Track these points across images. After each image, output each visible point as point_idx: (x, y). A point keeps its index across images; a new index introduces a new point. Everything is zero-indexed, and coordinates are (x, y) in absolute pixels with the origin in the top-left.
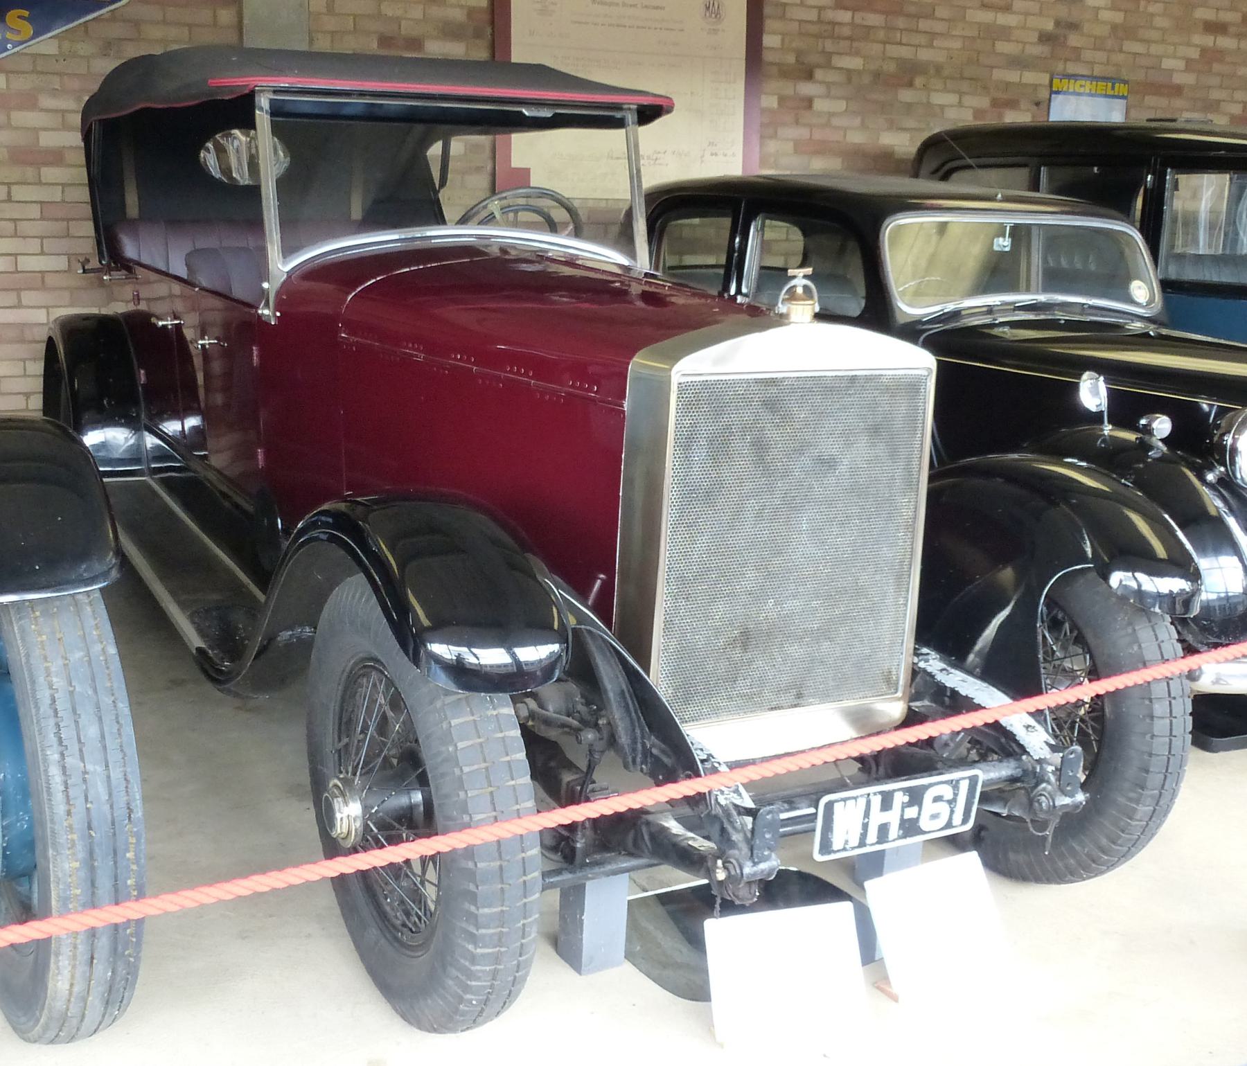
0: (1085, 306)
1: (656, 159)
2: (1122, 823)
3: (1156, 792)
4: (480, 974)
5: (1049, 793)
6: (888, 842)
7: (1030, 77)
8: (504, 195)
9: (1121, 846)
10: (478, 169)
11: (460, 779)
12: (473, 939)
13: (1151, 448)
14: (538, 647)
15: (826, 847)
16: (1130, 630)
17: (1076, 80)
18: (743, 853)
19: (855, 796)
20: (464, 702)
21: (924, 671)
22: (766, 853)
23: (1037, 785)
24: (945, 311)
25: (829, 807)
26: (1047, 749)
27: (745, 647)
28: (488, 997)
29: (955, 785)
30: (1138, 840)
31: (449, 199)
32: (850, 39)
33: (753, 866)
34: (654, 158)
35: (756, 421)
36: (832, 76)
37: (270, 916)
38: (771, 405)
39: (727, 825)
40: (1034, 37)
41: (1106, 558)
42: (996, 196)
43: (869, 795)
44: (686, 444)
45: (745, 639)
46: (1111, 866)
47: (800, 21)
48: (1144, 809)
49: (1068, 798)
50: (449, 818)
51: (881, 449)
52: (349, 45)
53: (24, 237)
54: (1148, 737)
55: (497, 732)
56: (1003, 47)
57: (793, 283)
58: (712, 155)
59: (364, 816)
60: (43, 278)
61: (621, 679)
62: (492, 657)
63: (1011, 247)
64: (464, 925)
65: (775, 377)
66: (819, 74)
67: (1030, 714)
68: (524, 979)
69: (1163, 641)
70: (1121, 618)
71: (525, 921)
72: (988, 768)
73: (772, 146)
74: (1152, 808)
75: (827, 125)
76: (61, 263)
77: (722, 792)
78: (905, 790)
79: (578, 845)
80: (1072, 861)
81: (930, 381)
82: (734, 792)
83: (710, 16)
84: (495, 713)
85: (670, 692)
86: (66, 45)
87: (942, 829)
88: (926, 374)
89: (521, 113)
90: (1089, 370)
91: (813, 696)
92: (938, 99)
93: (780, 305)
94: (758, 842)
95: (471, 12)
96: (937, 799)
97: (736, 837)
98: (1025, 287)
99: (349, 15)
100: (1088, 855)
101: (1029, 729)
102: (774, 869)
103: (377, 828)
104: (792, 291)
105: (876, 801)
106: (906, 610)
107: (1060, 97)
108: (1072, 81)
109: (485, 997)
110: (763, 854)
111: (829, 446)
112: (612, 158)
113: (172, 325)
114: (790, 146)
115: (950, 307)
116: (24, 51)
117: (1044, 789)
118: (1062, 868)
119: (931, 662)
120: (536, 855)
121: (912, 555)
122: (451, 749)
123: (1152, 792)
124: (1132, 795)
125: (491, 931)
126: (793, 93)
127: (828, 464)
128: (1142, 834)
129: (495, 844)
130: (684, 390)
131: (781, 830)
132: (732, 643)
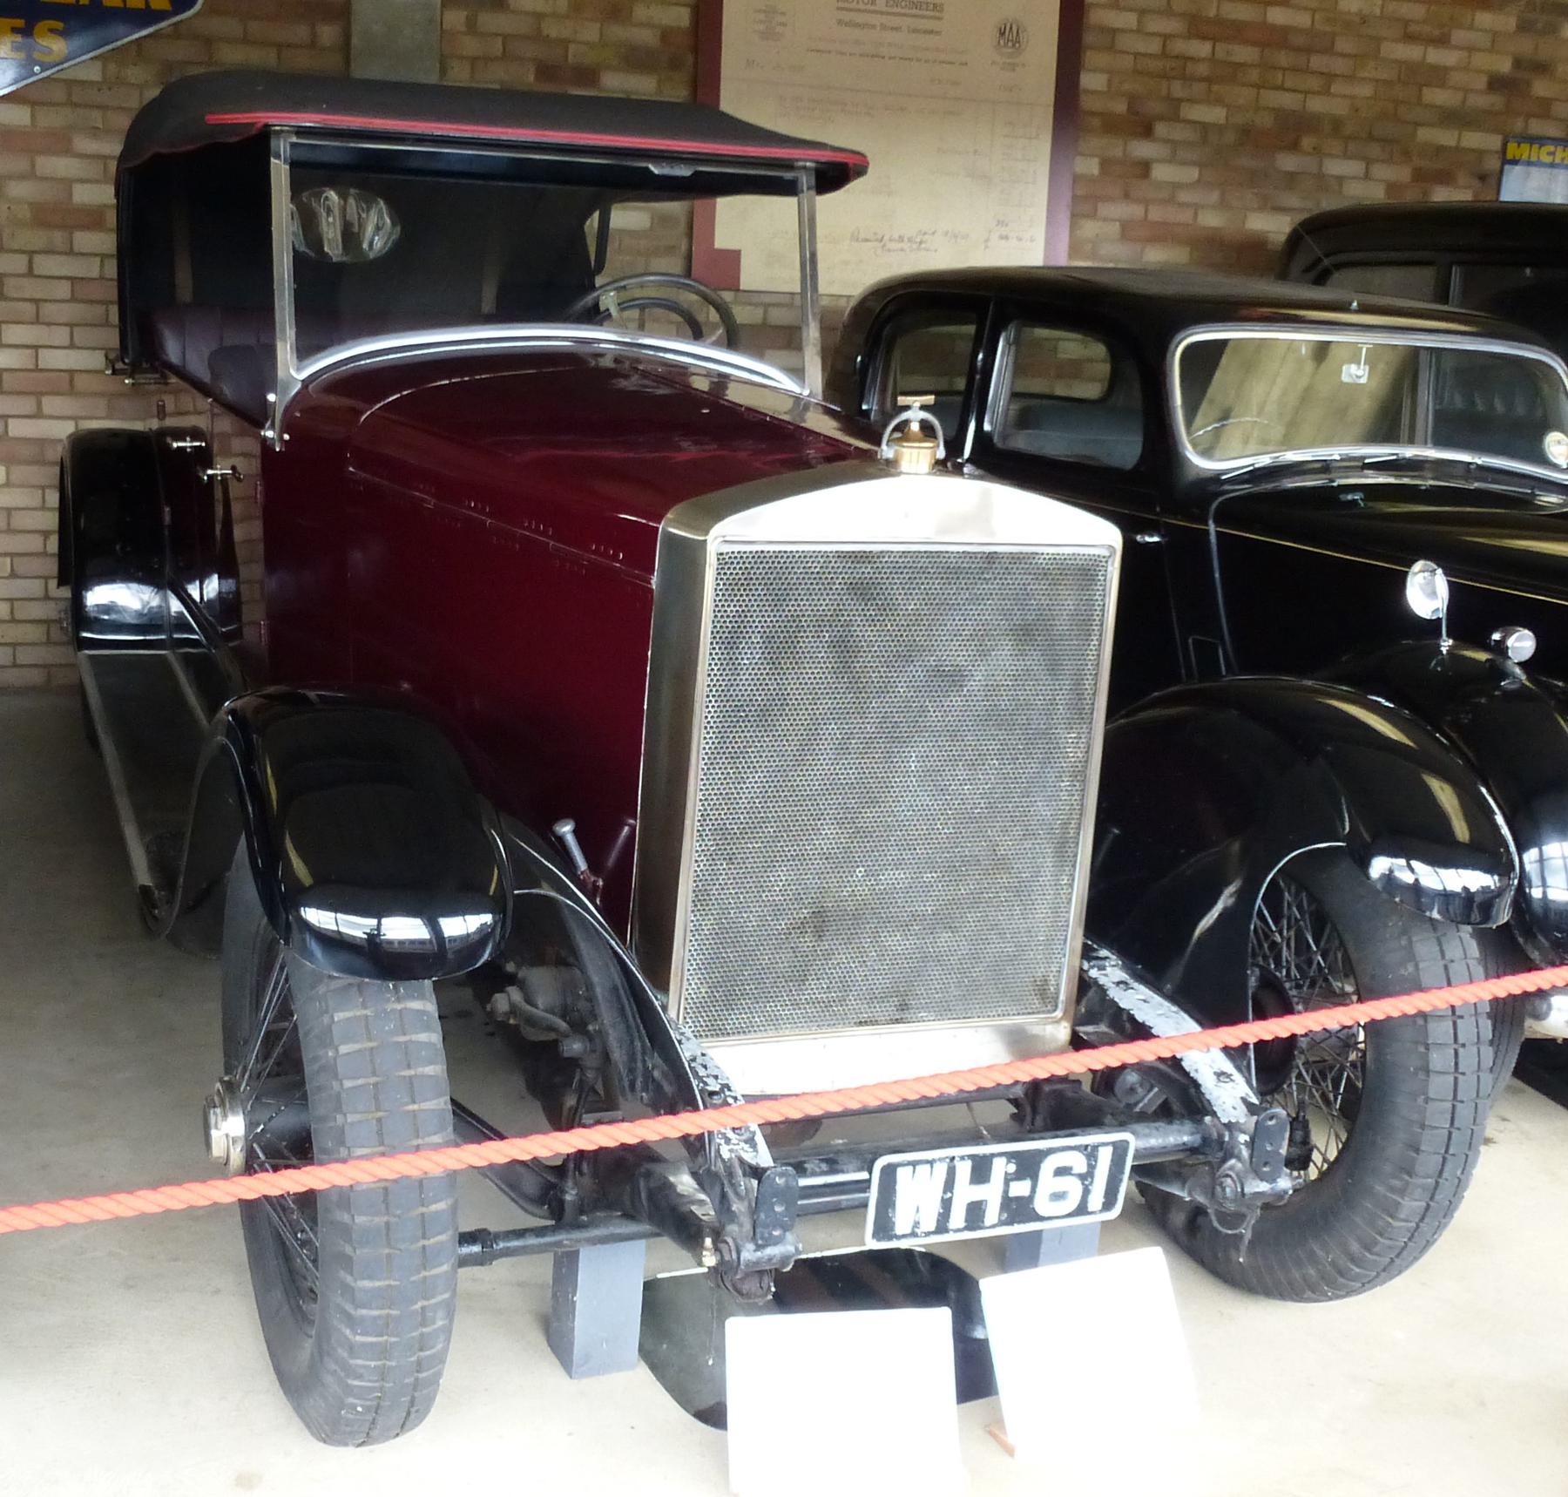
0: (1472, 467)
1: (921, 243)
3: (1431, 1181)
4: (362, 1371)
5: (1237, 1175)
6: (981, 1228)
7: (1474, 139)
8: (622, 284)
9: (1378, 1255)
10: (670, 250)
11: (338, 1096)
12: (351, 1321)
13: (1504, 674)
14: (467, 917)
15: (884, 1227)
16: (1404, 942)
17: (1541, 145)
18: (744, 1230)
19: (930, 1159)
20: (355, 989)
21: (1095, 981)
22: (776, 1233)
23: (1224, 1160)
24: (1257, 466)
25: (889, 1173)
26: (1243, 1109)
27: (819, 933)
28: (379, 1404)
29: (1091, 1153)
30: (1403, 1249)
32: (1209, 80)
33: (755, 1251)
34: (918, 240)
35: (838, 612)
36: (1179, 133)
37: (176, 1260)
38: (862, 590)
39: (727, 1189)
40: (1481, 82)
41: (1366, 835)
42: (1350, 304)
43: (953, 1159)
44: (730, 640)
45: (820, 922)
46: (1366, 1284)
47: (1137, 55)
48: (1411, 1205)
49: (1265, 1183)
50: (325, 1151)
51: (1034, 660)
52: (495, 77)
53: (49, 324)
54: (1421, 1099)
55: (398, 1035)
56: (1438, 97)
58: (1002, 237)
59: (246, 1137)
60: (71, 381)
61: (612, 969)
62: (403, 929)
63: (1369, 378)
64: (339, 1300)
65: (868, 550)
66: (1161, 129)
67: (1226, 1050)
68: (434, 1382)
69: (1452, 961)
70: (1394, 923)
71: (425, 1303)
72: (1147, 1131)
73: (1089, 228)
74: (1424, 1204)
75: (1171, 200)
76: (96, 360)
77: (728, 1141)
78: (1011, 1156)
79: (568, 1198)
80: (1312, 1272)
81: (1113, 565)
82: (746, 1142)
83: (1006, 45)
84: (399, 1007)
85: (703, 991)
86: (112, 67)
87: (1069, 1215)
88: (1107, 554)
89: (647, 168)
90: (1426, 558)
91: (926, 1007)
92: (1335, 167)
93: (884, 446)
94: (762, 1216)
95: (666, 34)
96: (1062, 1172)
97: (736, 1206)
98: (1406, 438)
99: (497, 35)
100: (1333, 1263)
101: (1221, 1078)
102: (791, 1257)
103: (265, 1154)
104: (902, 427)
105: (964, 1170)
106: (1070, 894)
107: (1518, 169)
108: (1535, 147)
109: (375, 1403)
110: (771, 1234)
111: (956, 655)
112: (857, 240)
113: (191, 447)
114: (1115, 228)
115: (1264, 461)
116: (55, 76)
117: (1231, 1168)
118: (1299, 1280)
119: (1109, 969)
120: (443, 1211)
121: (1081, 815)
122: (330, 1054)
123: (1424, 1181)
124: (1396, 1183)
125: (375, 1313)
126: (1121, 154)
127: (953, 678)
128: (1410, 1239)
129: (417, 1184)
130: (726, 563)
131: (799, 1203)
132: (801, 927)
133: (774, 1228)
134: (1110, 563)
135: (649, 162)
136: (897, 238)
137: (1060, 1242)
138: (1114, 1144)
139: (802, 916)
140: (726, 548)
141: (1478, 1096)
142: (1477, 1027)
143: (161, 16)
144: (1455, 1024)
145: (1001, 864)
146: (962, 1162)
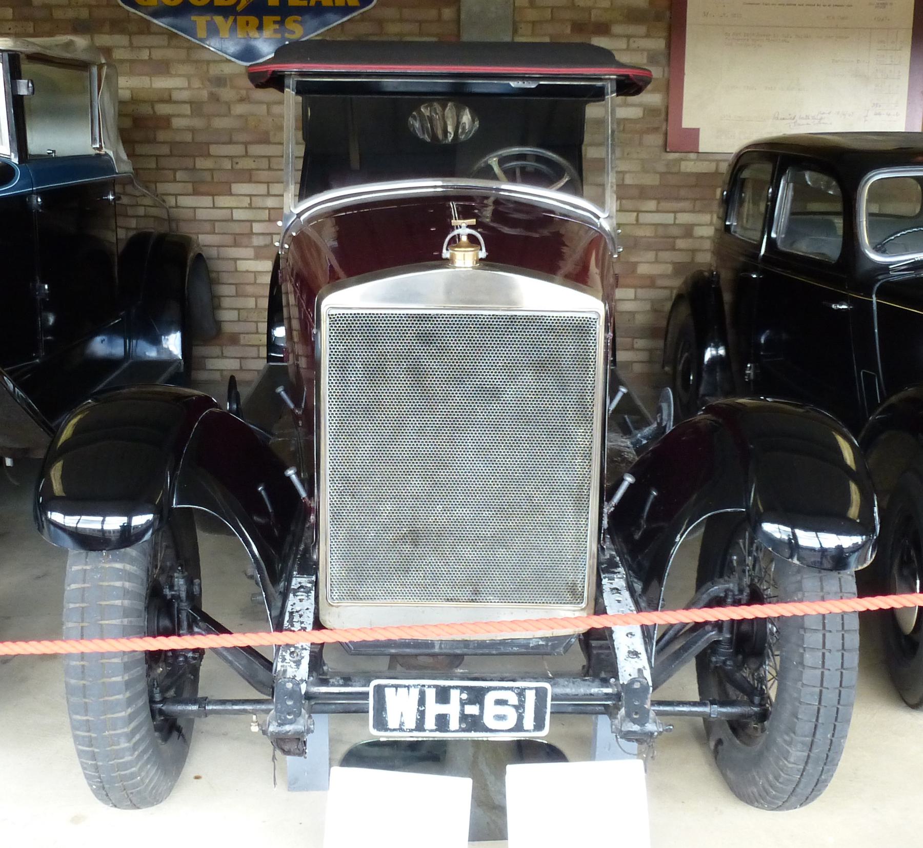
1: (821, 119)
2: (781, 763)
10: (656, 130)
15: (381, 723)
19: (407, 685)
24: (916, 259)
25: (379, 690)
27: (415, 543)
29: (521, 693)
31: (628, 154)
34: (819, 117)
38: (426, 338)
43: (424, 686)
44: (342, 365)
45: (414, 537)
49: (636, 726)
51: (550, 382)
57: (456, 232)
58: (876, 114)
78: (463, 689)
82: (294, 662)
93: (444, 251)
105: (431, 694)
110: (285, 717)
111: (495, 378)
112: (778, 119)
124: (787, 738)
133: (289, 714)
134: (597, 322)
135: (510, 80)
136: (805, 117)
137: (609, 749)
138: (536, 689)
139: (403, 532)
140: (334, 312)
141: (841, 686)
142: (843, 640)
143: (354, 9)
144: (824, 635)
145: (536, 509)
146: (430, 689)
